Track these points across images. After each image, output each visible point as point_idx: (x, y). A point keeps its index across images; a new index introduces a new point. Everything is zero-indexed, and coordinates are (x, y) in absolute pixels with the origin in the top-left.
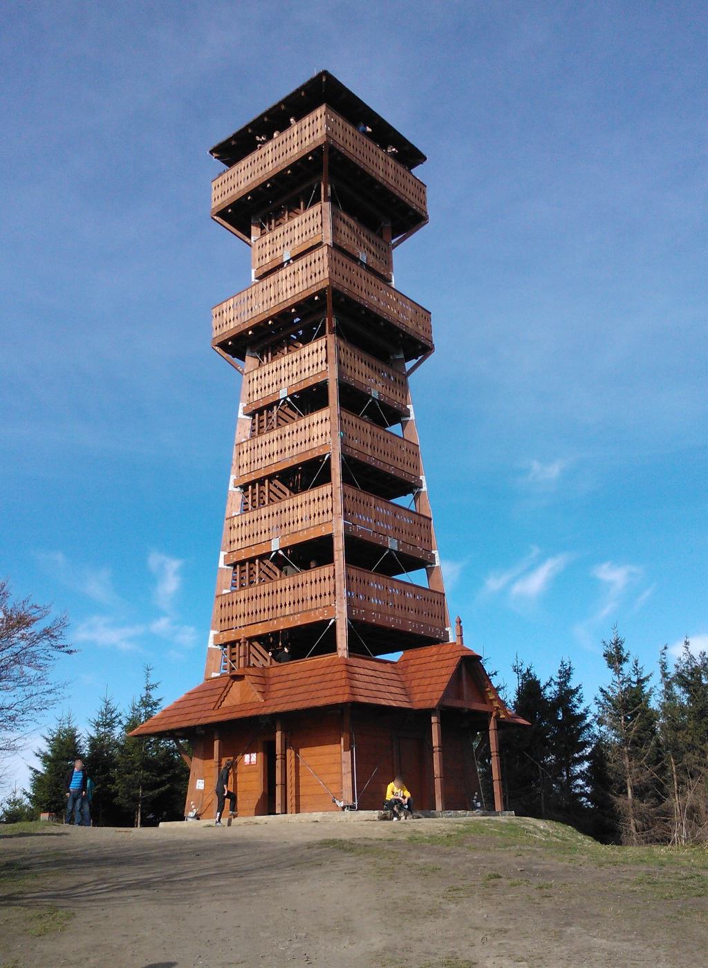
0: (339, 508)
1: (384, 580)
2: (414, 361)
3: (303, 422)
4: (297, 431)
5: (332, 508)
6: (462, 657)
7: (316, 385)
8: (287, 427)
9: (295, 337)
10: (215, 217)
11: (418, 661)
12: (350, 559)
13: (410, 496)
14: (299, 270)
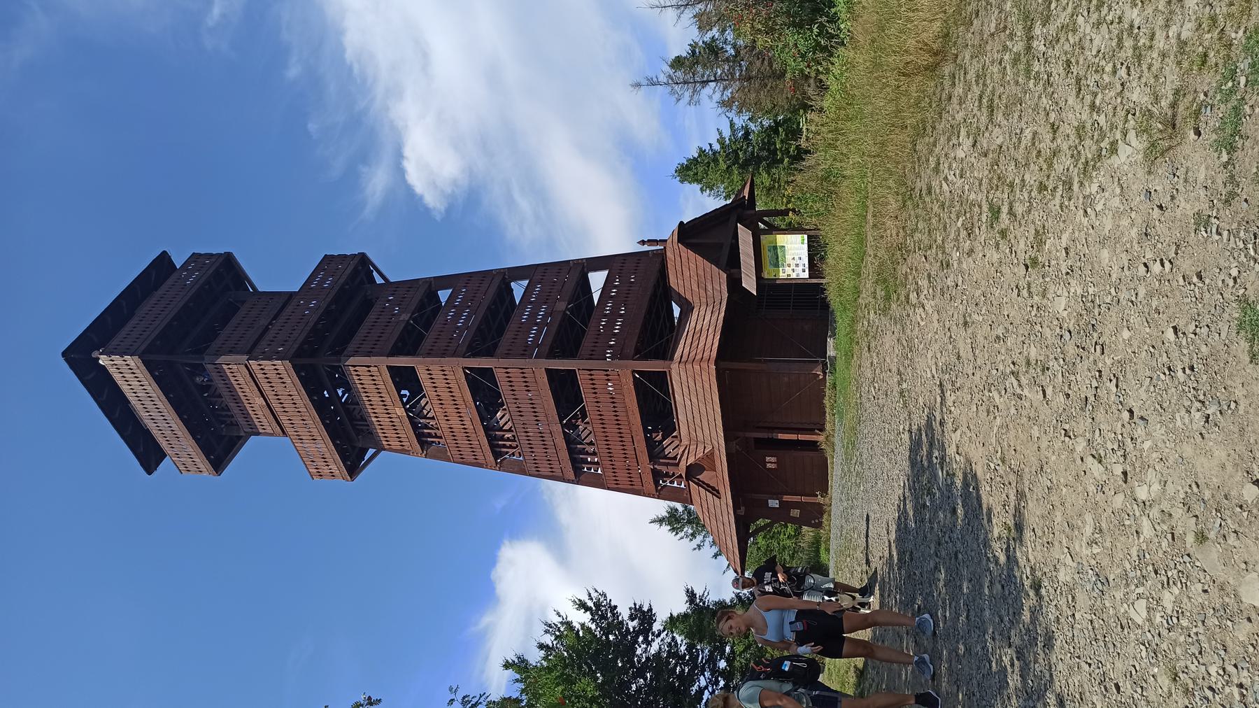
0: (520, 362)
2: (375, 273)
4: (440, 400)
5: (587, 370)
6: (678, 242)
9: (325, 392)
12: (572, 354)
14: (273, 391)
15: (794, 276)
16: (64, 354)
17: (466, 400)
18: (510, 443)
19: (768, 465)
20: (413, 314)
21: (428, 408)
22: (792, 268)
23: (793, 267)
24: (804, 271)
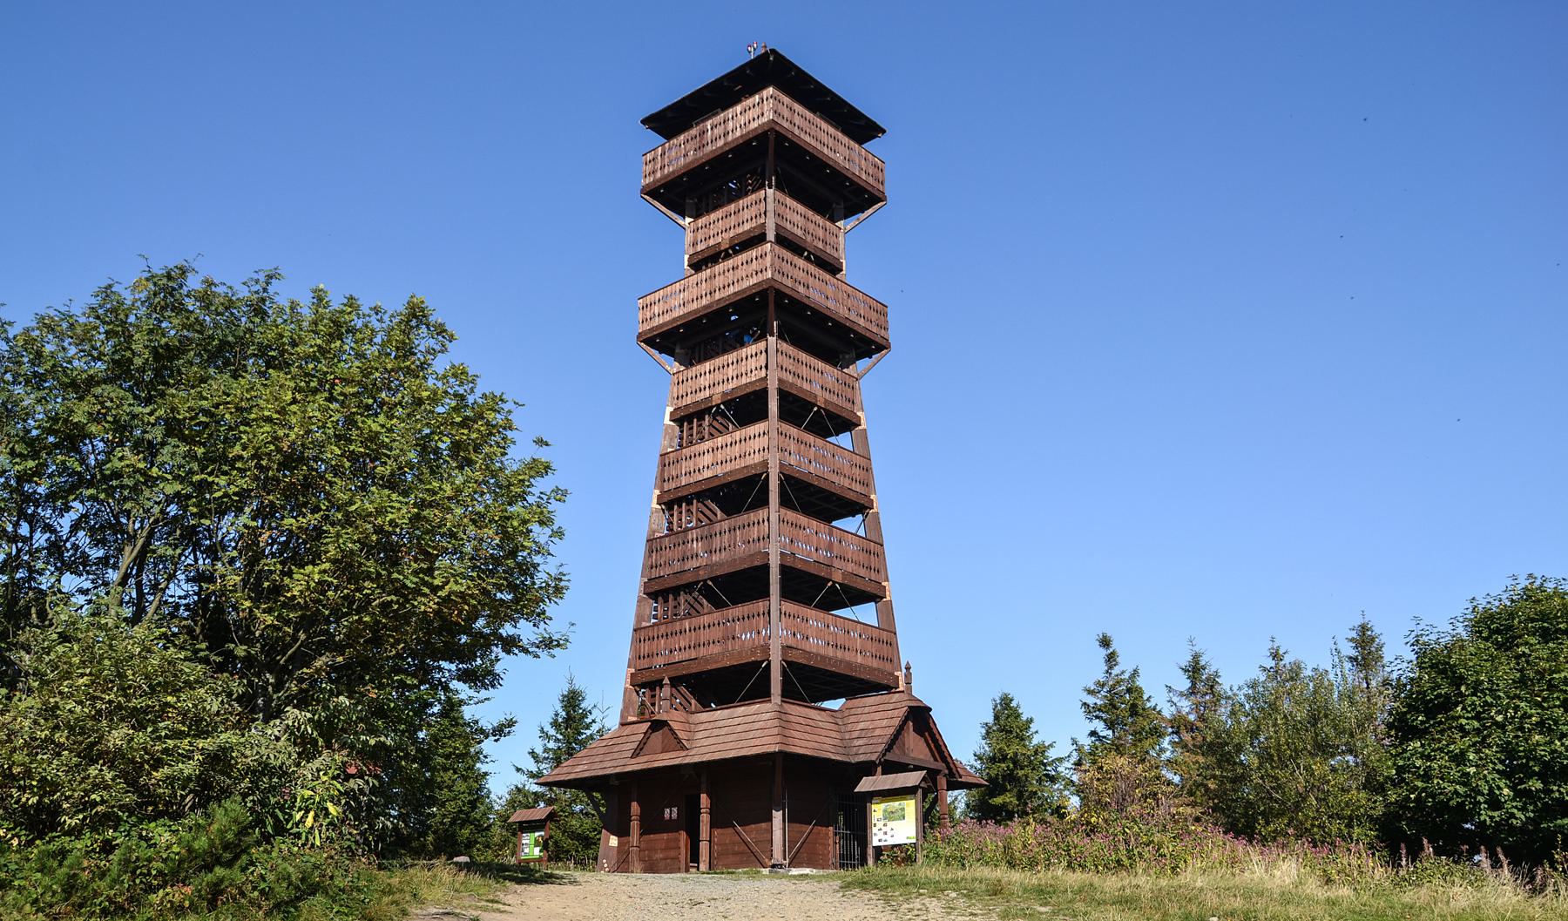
1: (821, 615)
3: (737, 435)
7: (755, 393)
8: (720, 439)
10: (646, 197)
11: (859, 711)
13: (859, 517)
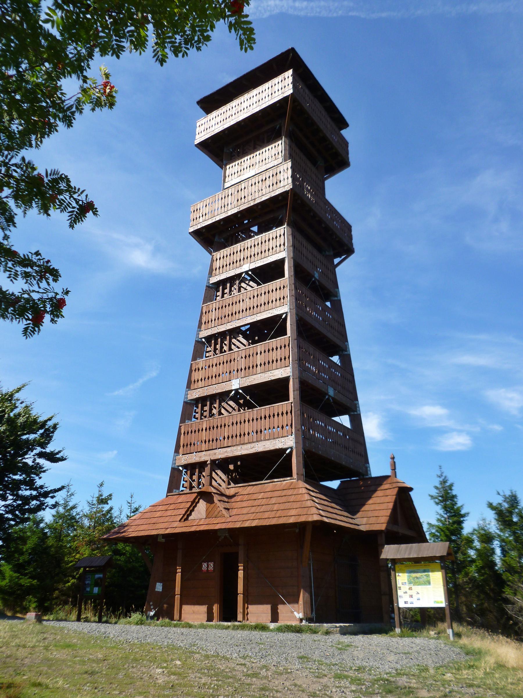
15: (400, 593)
16: (293, 50)
17: (258, 315)
18: (219, 349)
19: (206, 564)
20: (318, 281)
21: (249, 288)
22: (408, 591)
23: (410, 592)
24: (406, 603)
